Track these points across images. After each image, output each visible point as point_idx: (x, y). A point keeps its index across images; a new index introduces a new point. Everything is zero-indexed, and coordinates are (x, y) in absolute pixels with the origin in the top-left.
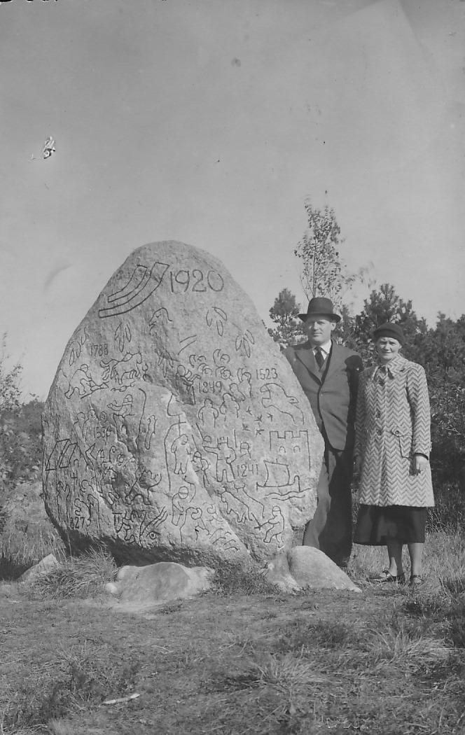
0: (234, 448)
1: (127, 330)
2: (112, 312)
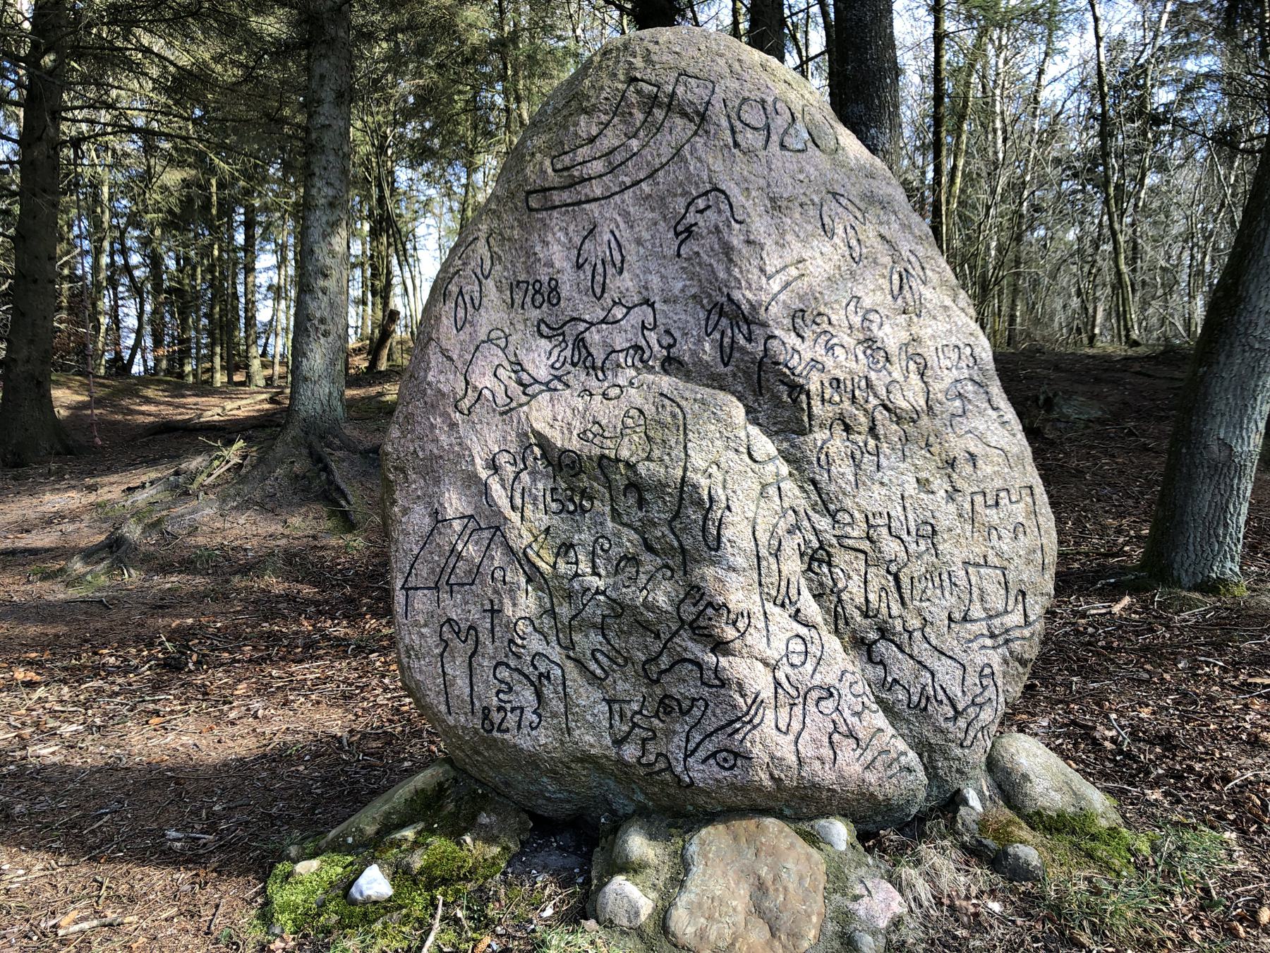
0: (905, 537)
1: (613, 244)
2: (566, 196)
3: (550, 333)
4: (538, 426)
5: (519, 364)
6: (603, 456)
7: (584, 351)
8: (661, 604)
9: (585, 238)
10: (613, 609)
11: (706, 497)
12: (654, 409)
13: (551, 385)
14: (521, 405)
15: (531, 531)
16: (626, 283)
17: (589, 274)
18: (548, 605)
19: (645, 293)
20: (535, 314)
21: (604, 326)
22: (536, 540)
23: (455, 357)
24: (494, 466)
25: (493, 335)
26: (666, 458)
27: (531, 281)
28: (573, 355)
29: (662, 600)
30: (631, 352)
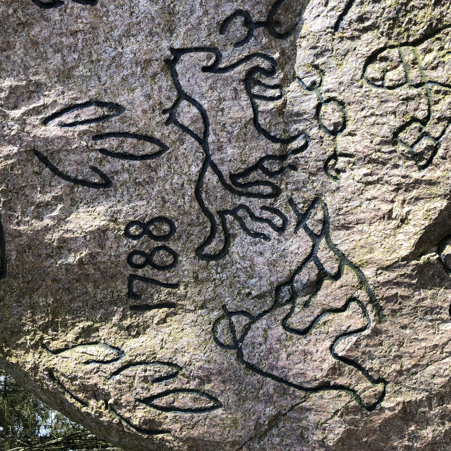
1: (68, 118)
3: (220, 236)
5: (278, 289)
7: (254, 176)
9: (55, 171)
12: (366, 37)
13: (317, 229)
14: (363, 282)
16: (139, 103)
17: (118, 164)
19: (155, 67)
20: (187, 263)
21: (211, 138)
23: (270, 411)
25: (226, 339)
27: (130, 271)
28: (260, 195)
30: (256, 90)
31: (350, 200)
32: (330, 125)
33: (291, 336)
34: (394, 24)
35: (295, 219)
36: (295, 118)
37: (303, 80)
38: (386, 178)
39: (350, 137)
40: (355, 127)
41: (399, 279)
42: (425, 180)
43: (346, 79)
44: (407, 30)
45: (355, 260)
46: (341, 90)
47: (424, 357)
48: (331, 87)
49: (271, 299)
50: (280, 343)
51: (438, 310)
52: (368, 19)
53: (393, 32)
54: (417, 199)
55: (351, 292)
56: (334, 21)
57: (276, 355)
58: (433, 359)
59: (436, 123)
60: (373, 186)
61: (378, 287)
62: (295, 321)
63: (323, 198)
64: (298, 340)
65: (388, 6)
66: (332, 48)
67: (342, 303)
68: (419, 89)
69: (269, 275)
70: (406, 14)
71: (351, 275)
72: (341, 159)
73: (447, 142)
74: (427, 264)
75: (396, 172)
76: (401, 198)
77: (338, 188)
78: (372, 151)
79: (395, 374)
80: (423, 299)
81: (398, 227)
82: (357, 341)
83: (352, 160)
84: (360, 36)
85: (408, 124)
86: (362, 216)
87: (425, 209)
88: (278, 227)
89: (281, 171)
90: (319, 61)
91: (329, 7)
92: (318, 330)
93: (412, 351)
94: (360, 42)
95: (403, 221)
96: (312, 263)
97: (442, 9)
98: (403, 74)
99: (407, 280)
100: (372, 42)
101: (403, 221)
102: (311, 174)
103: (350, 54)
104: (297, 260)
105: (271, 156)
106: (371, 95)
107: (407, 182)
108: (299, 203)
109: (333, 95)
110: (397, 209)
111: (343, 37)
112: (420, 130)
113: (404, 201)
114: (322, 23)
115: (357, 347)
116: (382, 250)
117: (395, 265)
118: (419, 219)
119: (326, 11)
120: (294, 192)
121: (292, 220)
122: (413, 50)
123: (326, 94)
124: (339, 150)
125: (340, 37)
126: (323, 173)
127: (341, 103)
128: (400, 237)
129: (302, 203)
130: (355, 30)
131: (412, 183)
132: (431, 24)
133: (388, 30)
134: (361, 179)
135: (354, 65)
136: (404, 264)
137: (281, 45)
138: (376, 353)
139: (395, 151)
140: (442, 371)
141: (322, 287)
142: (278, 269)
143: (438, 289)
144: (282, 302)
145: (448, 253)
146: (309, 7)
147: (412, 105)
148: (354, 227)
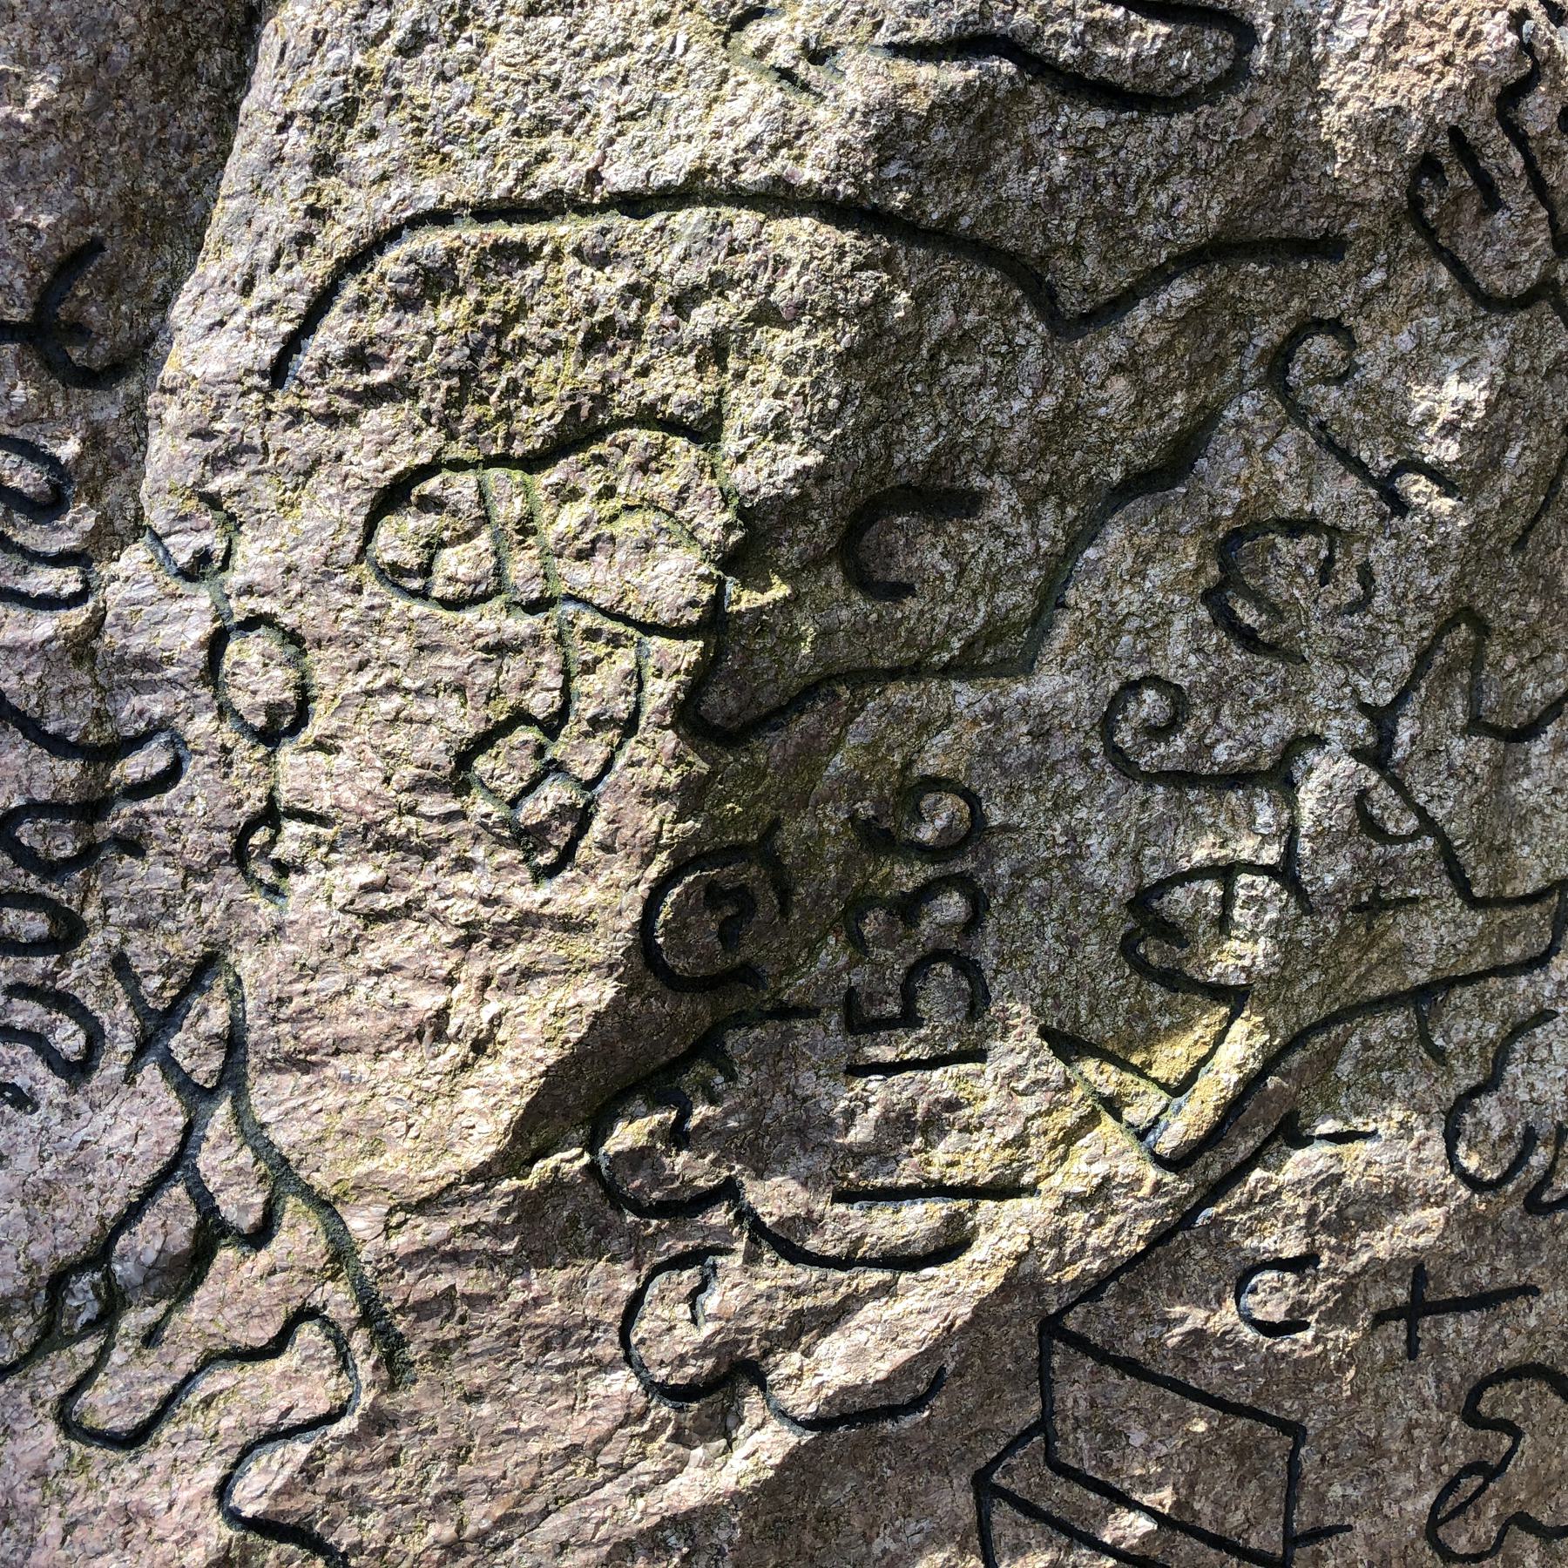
4: (482, 1117)
5: (59, 1282)
6: (687, 713)
8: (1474, 392)
10: (1449, 671)
11: (955, 75)
12: (379, 418)
13: (205, 1069)
14: (341, 1253)
15: (1071, 1136)
18: (1397, 1022)
22: (1113, 1105)
24: (715, 1392)
26: (703, 319)
29: (1458, 392)
31: (316, 970)
32: (254, 710)
33: (85, 1458)
34: (464, 388)
35: (132, 1030)
36: (136, 675)
37: (166, 541)
38: (433, 902)
39: (319, 757)
40: (335, 723)
41: (458, 1242)
42: (552, 916)
43: (308, 556)
44: (506, 415)
45: (319, 1180)
46: (292, 594)
47: (534, 1487)
48: (258, 578)
49: (30, 1320)
50: (45, 1485)
51: (586, 1333)
52: (382, 362)
53: (461, 417)
54: (528, 974)
55: (301, 1289)
56: (269, 352)
57: (27, 1528)
58: (563, 1492)
59: (586, 735)
60: (392, 925)
61: (391, 1270)
62: (106, 1405)
63: (232, 958)
64: (108, 1469)
65: (444, 327)
66: (265, 445)
67: (272, 1330)
68: (536, 620)
69: (24, 1237)
70: (502, 362)
71: (305, 1230)
72: (292, 827)
73: (617, 800)
74: (550, 1186)
75: (464, 882)
76: (476, 969)
77: (278, 928)
78: (387, 812)
79: (437, 1555)
80: (537, 1302)
81: (465, 1066)
82: (311, 1458)
83: (326, 833)
84: (357, 413)
85: (504, 728)
86: (352, 1026)
87: (551, 1007)
88: (67, 1062)
89: (87, 856)
90: (222, 483)
91: (254, 303)
92: (183, 1427)
93: (496, 1474)
94: (355, 436)
95: (479, 1047)
96: (178, 1191)
97: (609, 366)
98: (489, 563)
99: (485, 1243)
100: (393, 442)
101: (479, 1047)
102: (190, 871)
103: (323, 471)
104: (128, 1180)
105: (46, 804)
106: (389, 623)
107: (495, 919)
108: (147, 973)
109: (266, 606)
110: (463, 1005)
111: (301, 411)
112: (540, 751)
113: (486, 981)
114: (229, 351)
115: (311, 1479)
116: (409, 1144)
117: (447, 1197)
118: (528, 1041)
119: (246, 310)
120: (132, 934)
121: (121, 1033)
122: (524, 484)
123: (244, 599)
124: (284, 798)
125: (290, 410)
126: (232, 870)
127: (293, 638)
128: (470, 1099)
129: (160, 972)
130: (340, 391)
131: (511, 922)
132: (575, 410)
133: (445, 406)
134: (352, 902)
135: (336, 513)
136: (476, 1193)
137: (87, 410)
138: (376, 1492)
139: (461, 815)
140: (590, 1527)
141: (211, 1272)
142: (58, 1213)
143: (587, 1263)
144: (70, 1327)
145: (619, 1148)
146: (190, 288)
147: (515, 668)
148: (326, 1064)
